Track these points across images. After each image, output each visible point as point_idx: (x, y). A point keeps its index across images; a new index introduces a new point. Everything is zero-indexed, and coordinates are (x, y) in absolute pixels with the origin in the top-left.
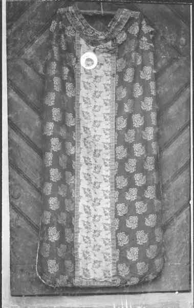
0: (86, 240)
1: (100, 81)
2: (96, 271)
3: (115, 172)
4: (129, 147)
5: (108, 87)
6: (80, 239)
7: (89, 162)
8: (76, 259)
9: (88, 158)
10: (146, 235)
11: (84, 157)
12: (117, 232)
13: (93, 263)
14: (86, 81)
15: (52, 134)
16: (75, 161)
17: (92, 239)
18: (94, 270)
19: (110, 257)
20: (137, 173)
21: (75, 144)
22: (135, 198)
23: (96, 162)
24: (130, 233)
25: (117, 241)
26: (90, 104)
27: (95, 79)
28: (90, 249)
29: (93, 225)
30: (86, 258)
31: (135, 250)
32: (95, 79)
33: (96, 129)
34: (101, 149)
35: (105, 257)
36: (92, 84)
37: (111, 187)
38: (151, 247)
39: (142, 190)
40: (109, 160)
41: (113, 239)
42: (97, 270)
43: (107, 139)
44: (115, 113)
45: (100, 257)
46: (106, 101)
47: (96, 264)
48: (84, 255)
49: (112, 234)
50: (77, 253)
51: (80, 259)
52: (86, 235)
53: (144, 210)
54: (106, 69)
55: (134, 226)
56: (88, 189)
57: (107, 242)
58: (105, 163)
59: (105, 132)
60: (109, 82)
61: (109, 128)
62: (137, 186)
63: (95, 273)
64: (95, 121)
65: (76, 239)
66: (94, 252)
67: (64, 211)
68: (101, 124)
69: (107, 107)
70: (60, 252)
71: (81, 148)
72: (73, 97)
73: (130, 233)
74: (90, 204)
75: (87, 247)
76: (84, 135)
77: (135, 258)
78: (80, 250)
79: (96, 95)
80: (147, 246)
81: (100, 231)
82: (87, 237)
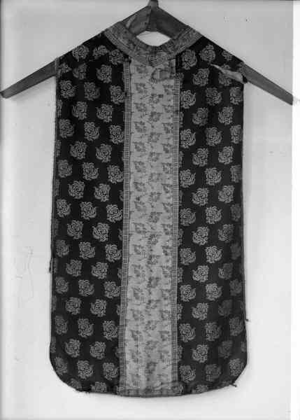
1: (158, 119)
3: (178, 243)
4: (200, 173)
5: (168, 272)
6: (128, 335)
7: (142, 108)
8: (121, 361)
9: (137, 332)
10: (218, 329)
12: (179, 322)
14: (138, 244)
15: (81, 237)
16: (120, 305)
19: (169, 336)
20: (208, 364)
24: (198, 325)
25: (179, 335)
26: (145, 111)
27: (152, 116)
28: (140, 329)
30: (136, 339)
32: (152, 116)
35: (166, 90)
37: (174, 262)
38: (225, 188)
40: (171, 268)
41: (173, 332)
43: (169, 198)
45: (157, 187)
46: (166, 147)
48: (133, 357)
49: (173, 326)
50: (123, 354)
52: (140, 102)
53: (217, 218)
54: (166, 103)
55: (203, 359)
58: (165, 230)
59: (165, 189)
60: (171, 121)
61: (171, 203)
64: (152, 174)
65: (122, 334)
66: (151, 223)
69: (168, 155)
72: (121, 103)
73: (198, 325)
75: (141, 99)
76: (135, 194)
77: (203, 360)
78: (127, 350)
79: (154, 217)
80: (219, 302)
82: (141, 104)
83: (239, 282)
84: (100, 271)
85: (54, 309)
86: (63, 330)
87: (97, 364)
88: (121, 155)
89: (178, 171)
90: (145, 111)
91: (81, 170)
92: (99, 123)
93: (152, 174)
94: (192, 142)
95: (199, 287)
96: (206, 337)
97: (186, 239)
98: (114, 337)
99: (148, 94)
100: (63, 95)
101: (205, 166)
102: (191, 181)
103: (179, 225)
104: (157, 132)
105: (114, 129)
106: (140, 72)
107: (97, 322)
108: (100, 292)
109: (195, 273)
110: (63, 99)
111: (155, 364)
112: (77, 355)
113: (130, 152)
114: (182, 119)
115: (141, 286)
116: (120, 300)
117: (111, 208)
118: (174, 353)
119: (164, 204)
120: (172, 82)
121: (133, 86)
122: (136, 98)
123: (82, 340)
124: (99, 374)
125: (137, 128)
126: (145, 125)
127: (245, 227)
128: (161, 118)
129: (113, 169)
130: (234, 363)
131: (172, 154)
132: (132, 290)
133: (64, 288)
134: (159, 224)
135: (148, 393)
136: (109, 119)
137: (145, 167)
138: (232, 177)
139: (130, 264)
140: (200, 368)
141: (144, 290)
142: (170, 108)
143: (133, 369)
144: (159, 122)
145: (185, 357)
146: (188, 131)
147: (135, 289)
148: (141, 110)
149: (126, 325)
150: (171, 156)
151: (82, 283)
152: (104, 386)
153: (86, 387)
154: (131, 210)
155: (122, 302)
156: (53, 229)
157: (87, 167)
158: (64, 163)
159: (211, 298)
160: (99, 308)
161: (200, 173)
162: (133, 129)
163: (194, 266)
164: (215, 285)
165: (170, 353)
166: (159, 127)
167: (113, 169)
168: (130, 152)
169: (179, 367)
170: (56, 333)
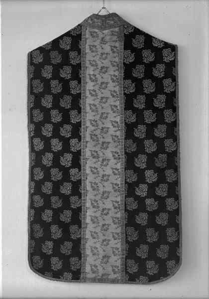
0: (92, 47)
2: (103, 47)
7: (96, 251)
11: (91, 183)
13: (102, 258)
17: (100, 235)
18: (101, 46)
19: (118, 270)
21: (81, 139)
22: (145, 194)
23: (104, 154)
28: (98, 245)
29: (100, 123)
31: (144, 216)
32: (103, 178)
33: (104, 135)
34: (108, 66)
36: (98, 75)
39: (151, 127)
42: (106, 184)
44: (125, 193)
47: (105, 243)
48: (92, 251)
51: (88, 255)
56: (93, 75)
57: (115, 50)
62: (145, 93)
63: (102, 49)
64: (102, 113)
67: (69, 93)
68: (110, 212)
70: (63, 132)
71: (87, 142)
73: (141, 201)
74: (97, 149)
81: (109, 160)
82: (95, 232)
83: (174, 142)
84: (66, 189)
85: (32, 219)
86: (40, 234)
87: (65, 259)
88: (79, 159)
89: (124, 227)
90: (97, 126)
91: (49, 263)
92: (62, 80)
93: (102, 113)
94: (132, 90)
95: (141, 201)
96: (147, 239)
97: (130, 163)
98: (78, 92)
99: (98, 82)
100: (35, 120)
101: (142, 48)
102: (131, 59)
103: (125, 152)
104: (106, 82)
105: (73, 84)
106: (92, 52)
107: (66, 199)
108: (66, 148)
109: (137, 189)
110: (35, 209)
111: (109, 257)
112: (50, 192)
113: (86, 83)
114: (127, 190)
115: (95, 44)
116: (81, 209)
117: (72, 54)
118: (122, 250)
119: (113, 184)
120: (117, 44)
121: (87, 47)
122: (90, 86)
123: (54, 241)
124: (66, 267)
125: (91, 79)
126: (98, 170)
127: (183, 216)
128: (109, 101)
129: (73, 113)
130: (170, 263)
131: (119, 176)
132: (90, 201)
133: (40, 176)
134: (108, 167)
135: (103, 280)
136: (144, 166)
137: (98, 270)
138: (166, 148)
139: (87, 182)
140: (141, 263)
141: (99, 266)
142: (115, 64)
143: (90, 261)
144: (108, 200)
145: (131, 252)
146: (132, 199)
147: (91, 247)
148: (93, 37)
149: (86, 227)
150: (118, 242)
151: (54, 199)
152: (70, 276)
153: (57, 276)
154: (87, 126)
155: (83, 210)
156: (31, 160)
157: (54, 199)
158: (37, 227)
159: (148, 122)
160: (66, 216)
161: (138, 83)
162: (88, 80)
163: (137, 184)
164: (153, 262)
165: (120, 250)
166: (107, 77)
167: (73, 113)
168: (86, 83)
169: (126, 260)
170: (34, 237)
